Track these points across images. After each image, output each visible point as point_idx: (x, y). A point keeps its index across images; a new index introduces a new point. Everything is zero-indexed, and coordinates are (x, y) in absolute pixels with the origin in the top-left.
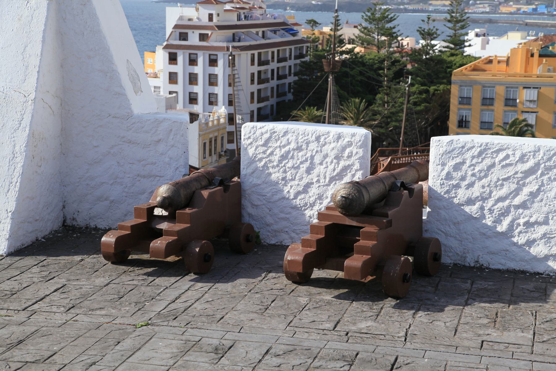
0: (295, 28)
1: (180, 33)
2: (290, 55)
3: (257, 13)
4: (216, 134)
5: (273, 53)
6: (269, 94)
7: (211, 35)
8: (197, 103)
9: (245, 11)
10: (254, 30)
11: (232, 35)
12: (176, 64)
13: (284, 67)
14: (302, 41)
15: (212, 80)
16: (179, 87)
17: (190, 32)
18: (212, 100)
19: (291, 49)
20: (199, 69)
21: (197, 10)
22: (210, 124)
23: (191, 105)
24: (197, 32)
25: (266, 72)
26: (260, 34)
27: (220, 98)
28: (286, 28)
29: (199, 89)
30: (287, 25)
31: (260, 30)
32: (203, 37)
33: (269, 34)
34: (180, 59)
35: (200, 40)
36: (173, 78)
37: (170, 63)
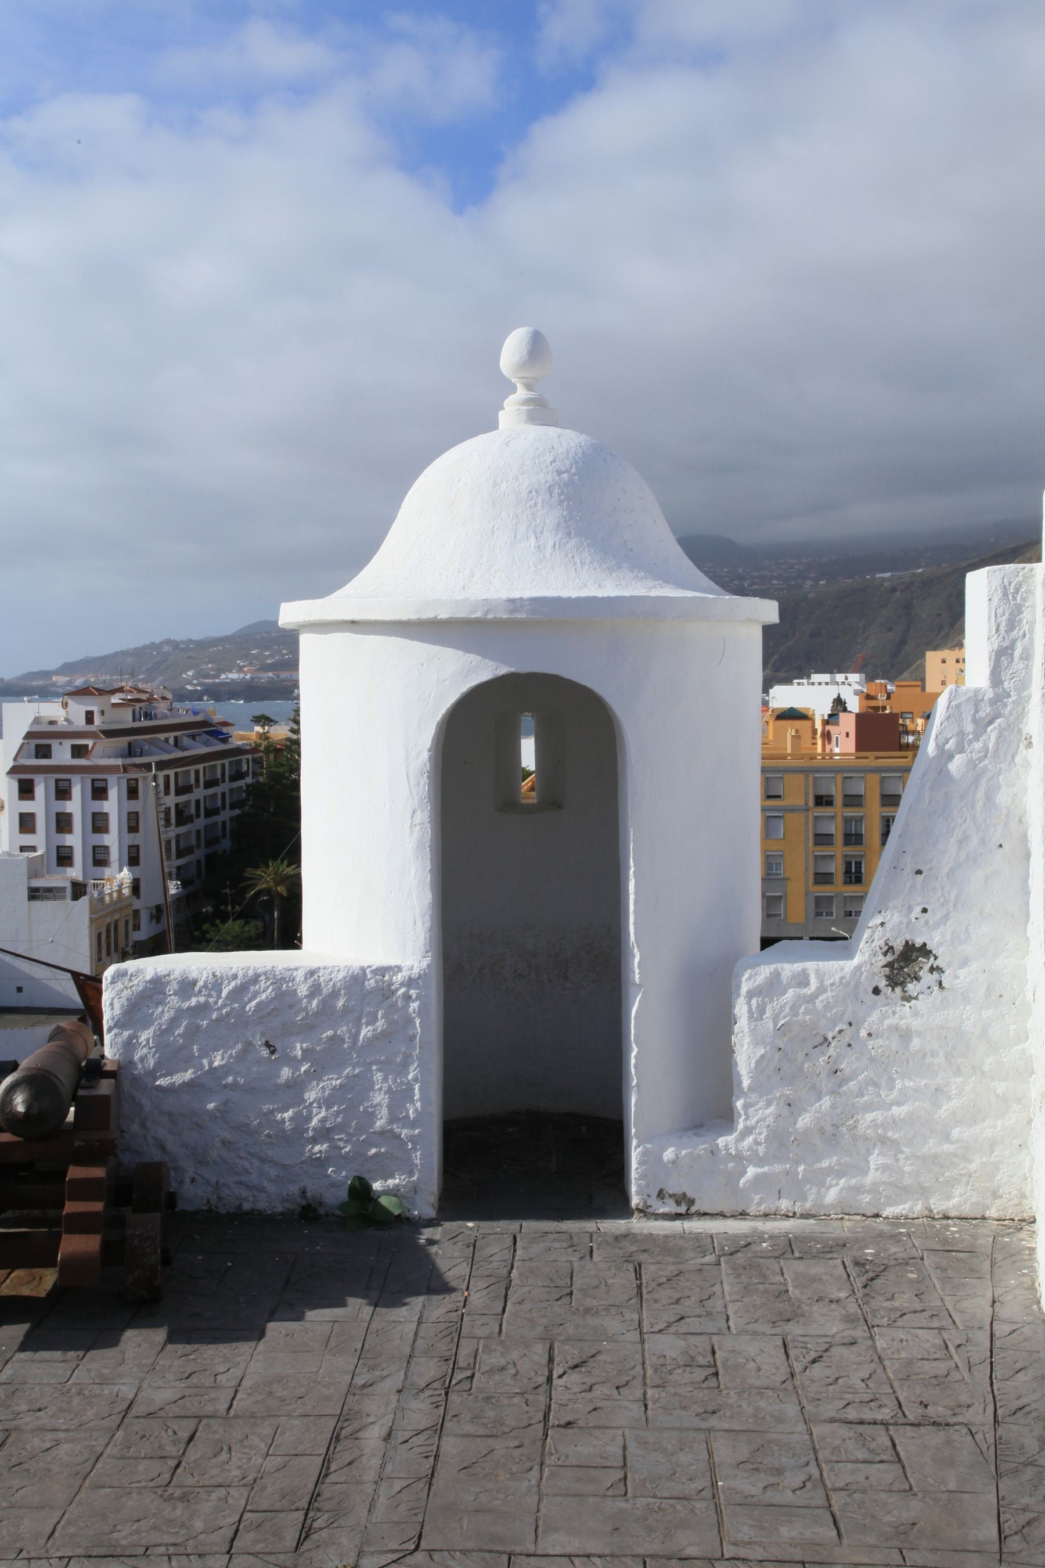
0: (225, 730)
1: (37, 746)
2: (223, 774)
3: (162, 707)
4: (116, 916)
5: (197, 772)
6: (193, 842)
7: (92, 748)
8: (71, 865)
9: (142, 705)
10: (162, 736)
11: (126, 745)
12: (33, 799)
13: (215, 795)
14: (239, 751)
15: (99, 824)
16: (38, 839)
17: (54, 744)
18: (99, 858)
19: (223, 765)
20: (74, 806)
21: (65, 705)
22: (107, 898)
23: (61, 868)
24: (68, 744)
25: (187, 804)
26: (172, 741)
27: (114, 855)
28: (215, 731)
29: (74, 840)
30: (211, 725)
31: (171, 736)
32: (78, 751)
33: (186, 741)
34: (40, 790)
35: (73, 756)
36: (26, 823)
37: (21, 798)
